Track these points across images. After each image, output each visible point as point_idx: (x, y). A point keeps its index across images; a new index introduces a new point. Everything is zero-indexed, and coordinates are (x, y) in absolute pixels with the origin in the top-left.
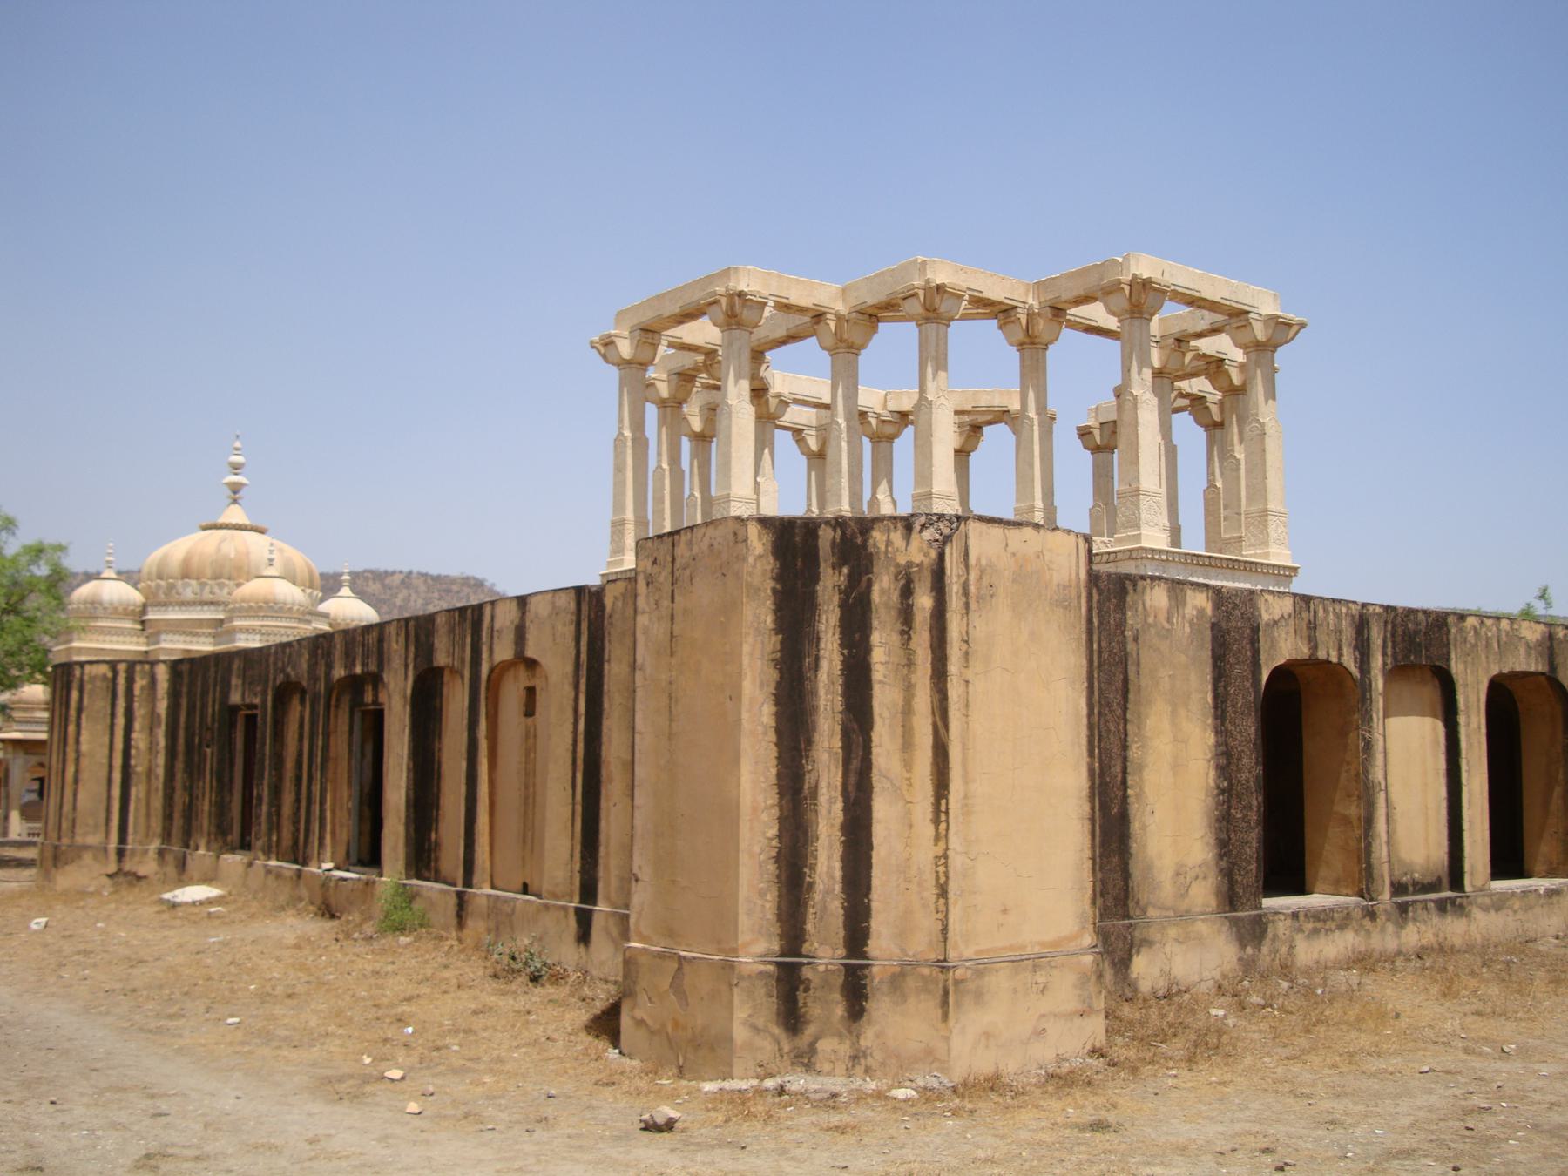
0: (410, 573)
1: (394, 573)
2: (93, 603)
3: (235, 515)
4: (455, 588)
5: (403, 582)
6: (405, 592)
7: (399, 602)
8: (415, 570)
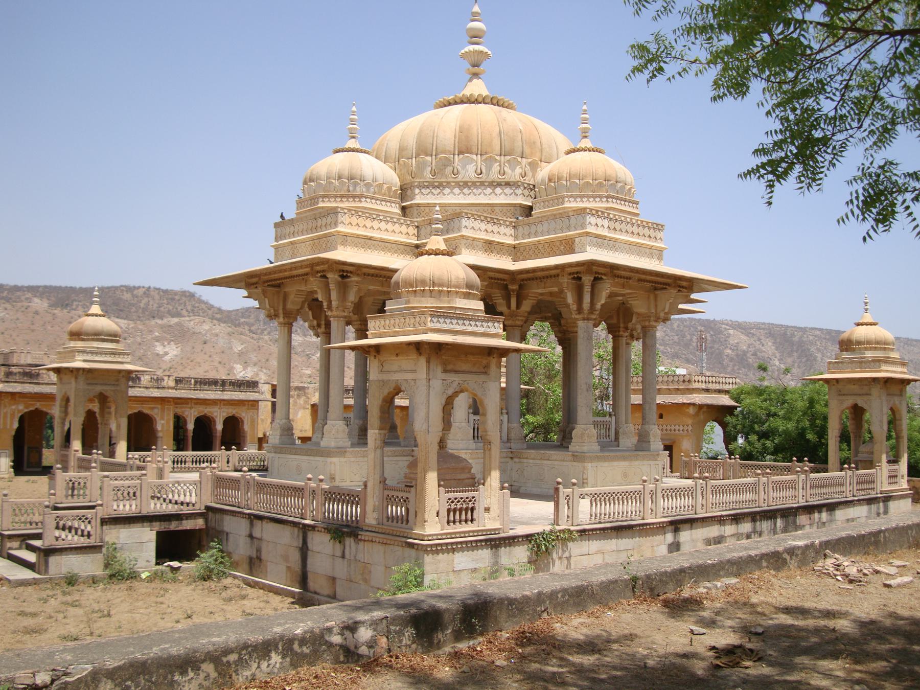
0: (149, 288)
1: (139, 288)
2: (351, 178)
3: (477, 88)
4: (177, 297)
5: (145, 293)
6: (146, 299)
7: (142, 305)
8: (152, 286)
